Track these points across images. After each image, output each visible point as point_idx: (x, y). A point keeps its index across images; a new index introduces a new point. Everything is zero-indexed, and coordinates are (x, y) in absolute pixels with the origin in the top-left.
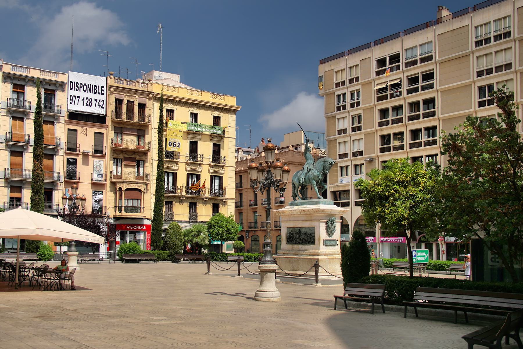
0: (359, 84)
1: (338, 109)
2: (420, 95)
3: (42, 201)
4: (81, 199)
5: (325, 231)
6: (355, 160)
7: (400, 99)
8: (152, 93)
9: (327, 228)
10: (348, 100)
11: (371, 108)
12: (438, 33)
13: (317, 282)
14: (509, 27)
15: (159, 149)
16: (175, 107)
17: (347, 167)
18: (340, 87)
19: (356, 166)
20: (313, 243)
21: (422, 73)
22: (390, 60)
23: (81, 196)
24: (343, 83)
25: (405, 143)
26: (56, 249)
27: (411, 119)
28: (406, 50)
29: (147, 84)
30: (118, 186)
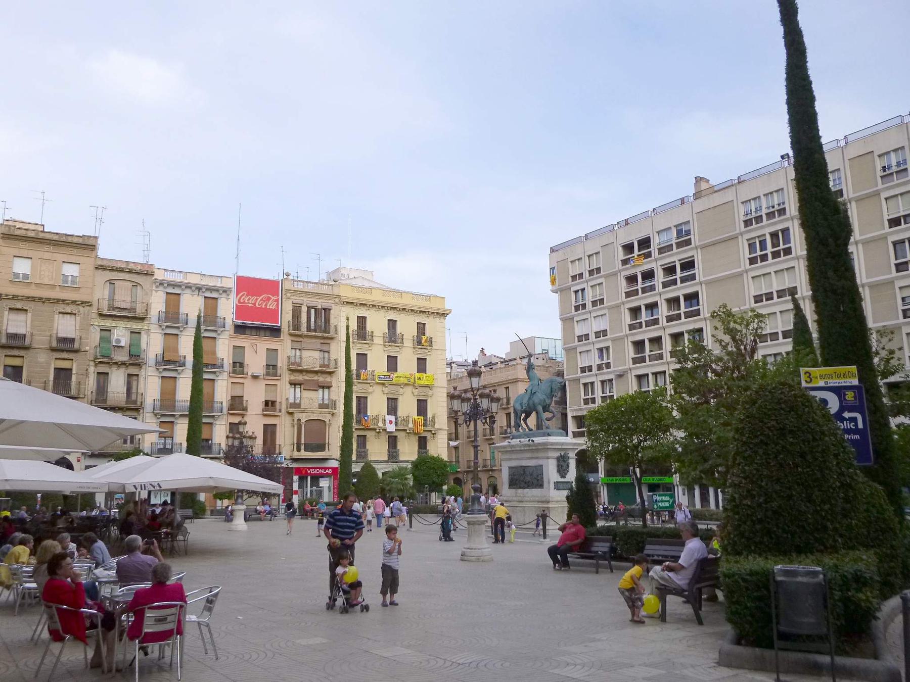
0: (601, 277)
1: (577, 308)
2: (679, 289)
3: (198, 445)
4: (251, 438)
5: (555, 470)
6: (601, 374)
7: (655, 295)
8: (339, 296)
11: (618, 306)
12: (696, 210)
14: (783, 203)
16: (368, 312)
17: (592, 383)
18: (578, 281)
19: (603, 382)
20: (541, 486)
22: (639, 245)
23: (250, 434)
24: (581, 275)
25: (664, 351)
26: (216, 502)
27: (670, 319)
28: (658, 232)
29: (332, 285)
30: (297, 416)
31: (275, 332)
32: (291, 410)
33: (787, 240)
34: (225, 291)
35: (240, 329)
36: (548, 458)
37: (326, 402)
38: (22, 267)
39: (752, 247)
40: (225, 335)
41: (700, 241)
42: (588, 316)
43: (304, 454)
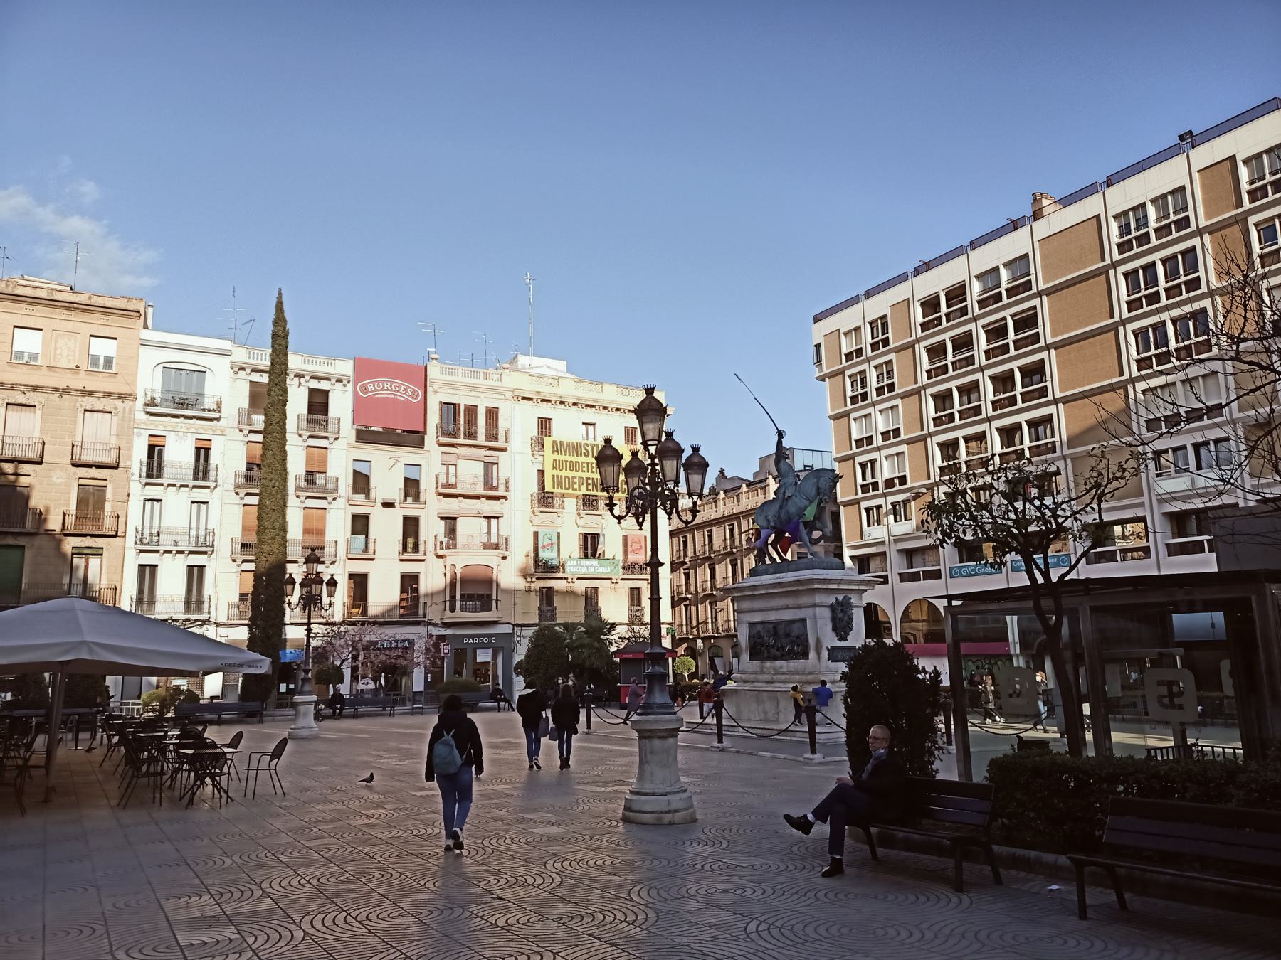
5: (829, 626)
9: (834, 619)
10: (873, 383)
13: (813, 752)
15: (274, 335)
21: (1012, 316)
30: (449, 561)
31: (414, 439)
32: (440, 552)
33: (1192, 266)
34: (339, 381)
35: (364, 436)
37: (494, 540)
38: (27, 342)
39: (1133, 287)
40: (341, 443)
42: (870, 410)
43: (460, 616)
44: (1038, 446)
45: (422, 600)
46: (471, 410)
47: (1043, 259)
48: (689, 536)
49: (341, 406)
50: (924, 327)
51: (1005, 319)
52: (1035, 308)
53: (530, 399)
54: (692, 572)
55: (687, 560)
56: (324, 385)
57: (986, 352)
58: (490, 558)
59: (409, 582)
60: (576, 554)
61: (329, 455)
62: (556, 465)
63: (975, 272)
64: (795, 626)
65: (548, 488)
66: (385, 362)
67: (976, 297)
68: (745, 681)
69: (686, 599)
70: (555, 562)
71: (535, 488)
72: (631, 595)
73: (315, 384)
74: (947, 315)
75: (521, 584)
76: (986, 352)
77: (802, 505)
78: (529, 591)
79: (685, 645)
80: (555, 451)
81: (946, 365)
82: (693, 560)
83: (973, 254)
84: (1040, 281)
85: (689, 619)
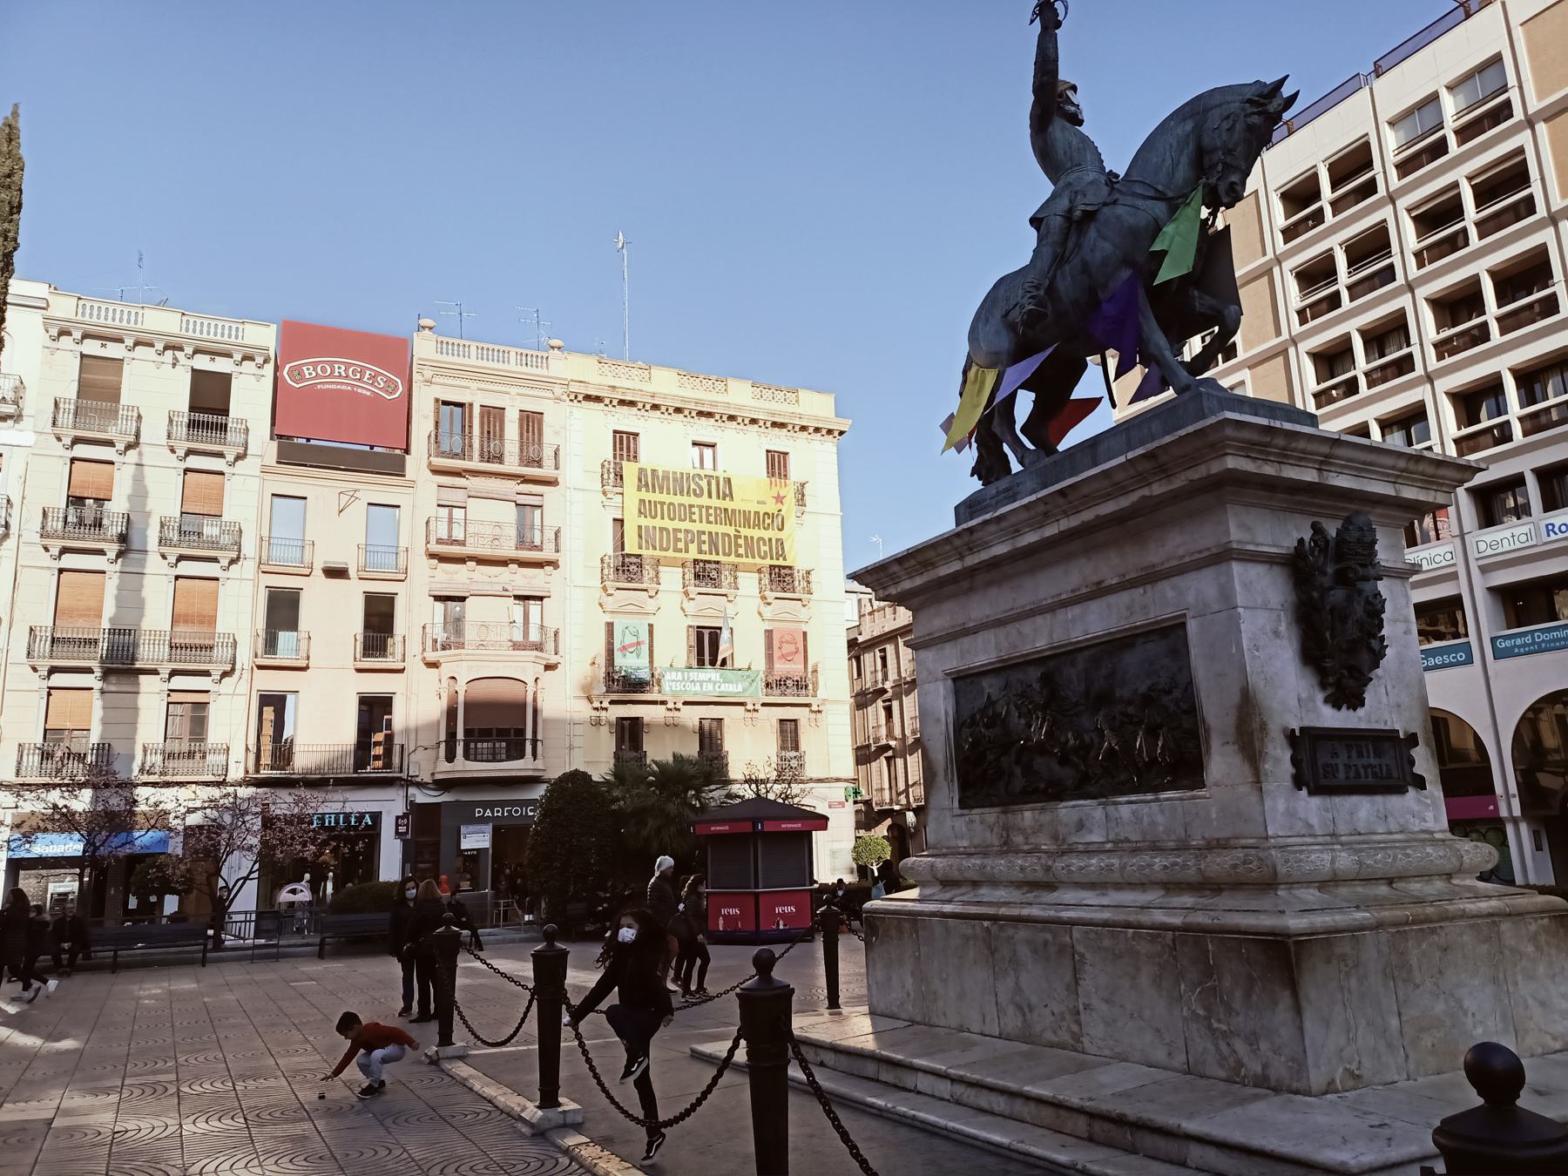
30: (446, 670)
32: (431, 656)
35: (293, 453)
36: (1224, 556)
37: (534, 636)
40: (249, 466)
41: (1541, 95)
43: (464, 767)
44: (1535, 415)
45: (397, 741)
46: (493, 416)
47: (1533, 56)
48: (890, 648)
49: (250, 401)
50: (1289, 233)
51: (1456, 185)
52: (1520, 151)
53: (598, 399)
54: (895, 704)
55: (888, 685)
56: (221, 365)
57: (1418, 255)
58: (525, 667)
59: (374, 710)
60: (682, 661)
61: (227, 484)
62: (645, 508)
63: (1386, 114)
64: (1132, 660)
65: (631, 547)
66: (333, 330)
67: (1392, 159)
68: (947, 883)
69: (888, 747)
70: (644, 674)
71: (608, 547)
72: (782, 732)
73: (203, 363)
74: (1333, 204)
75: (584, 711)
76: (1418, 255)
77: (1141, 220)
78: (597, 723)
79: (889, 822)
80: (642, 484)
81: (1337, 293)
82: (897, 686)
83: (1379, 84)
84: (1528, 96)
85: (893, 779)
